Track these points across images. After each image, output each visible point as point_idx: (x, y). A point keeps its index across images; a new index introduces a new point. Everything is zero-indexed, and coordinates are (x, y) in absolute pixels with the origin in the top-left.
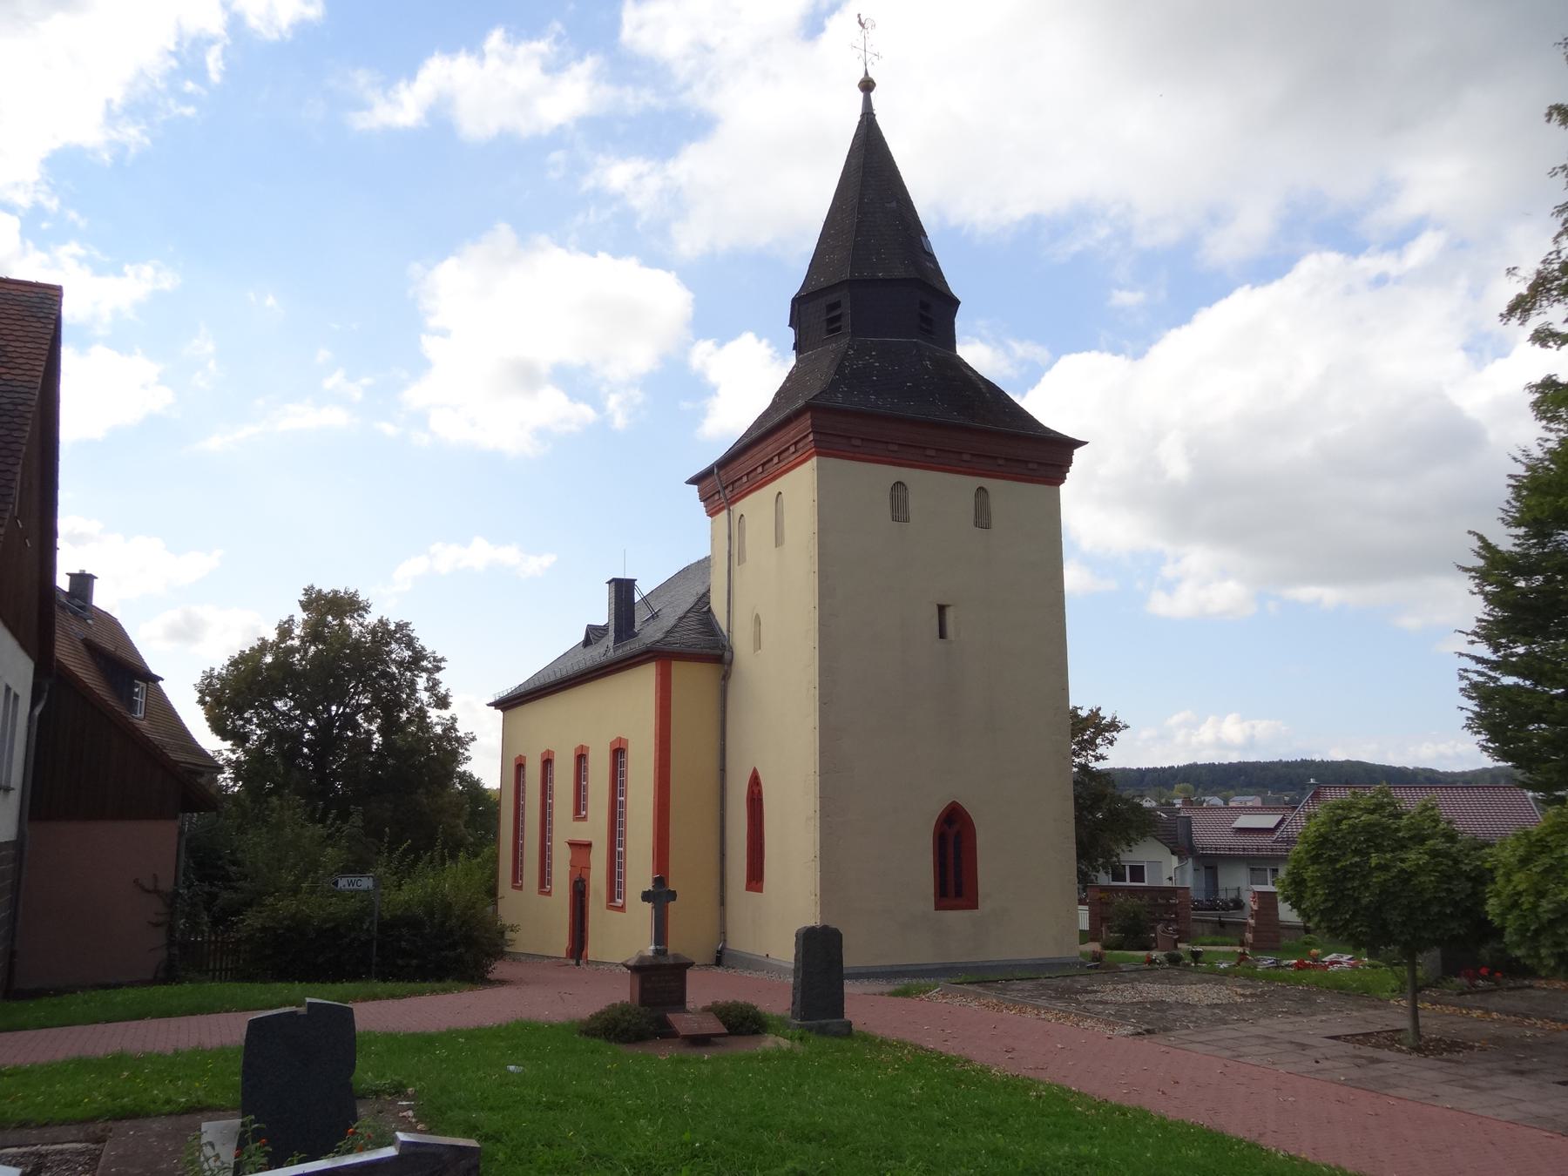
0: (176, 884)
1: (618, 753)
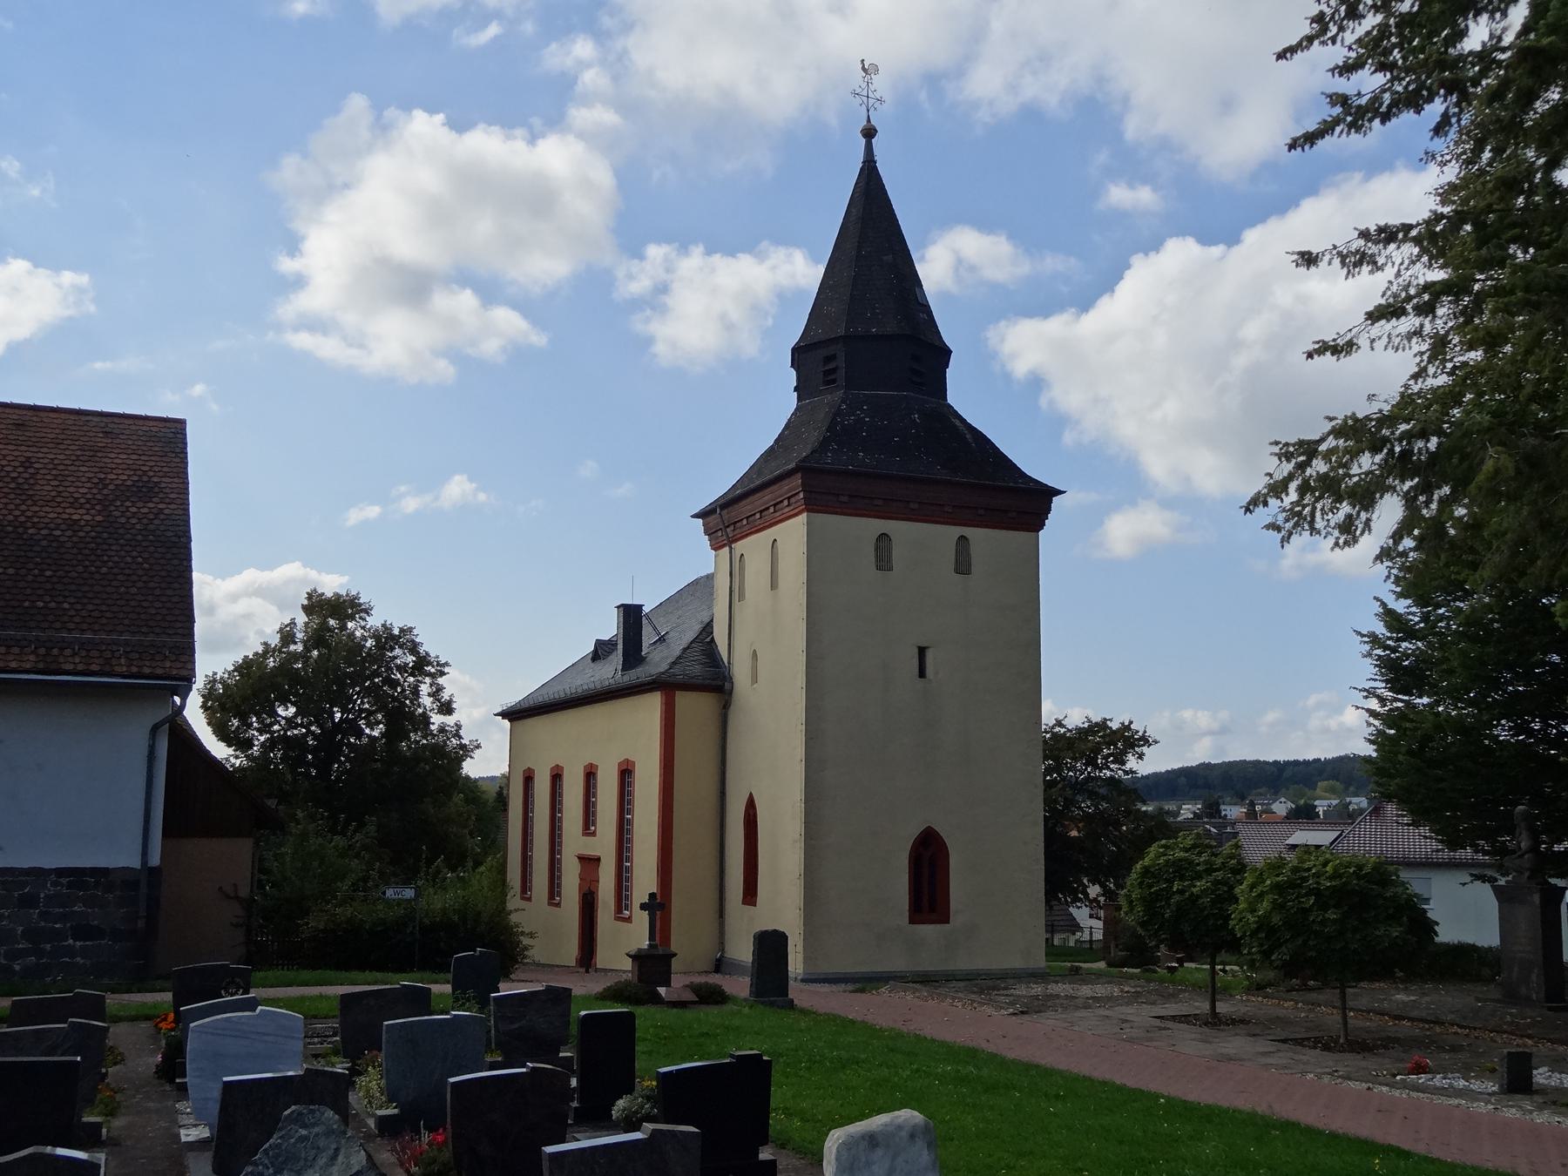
0: (252, 891)
1: (626, 773)
